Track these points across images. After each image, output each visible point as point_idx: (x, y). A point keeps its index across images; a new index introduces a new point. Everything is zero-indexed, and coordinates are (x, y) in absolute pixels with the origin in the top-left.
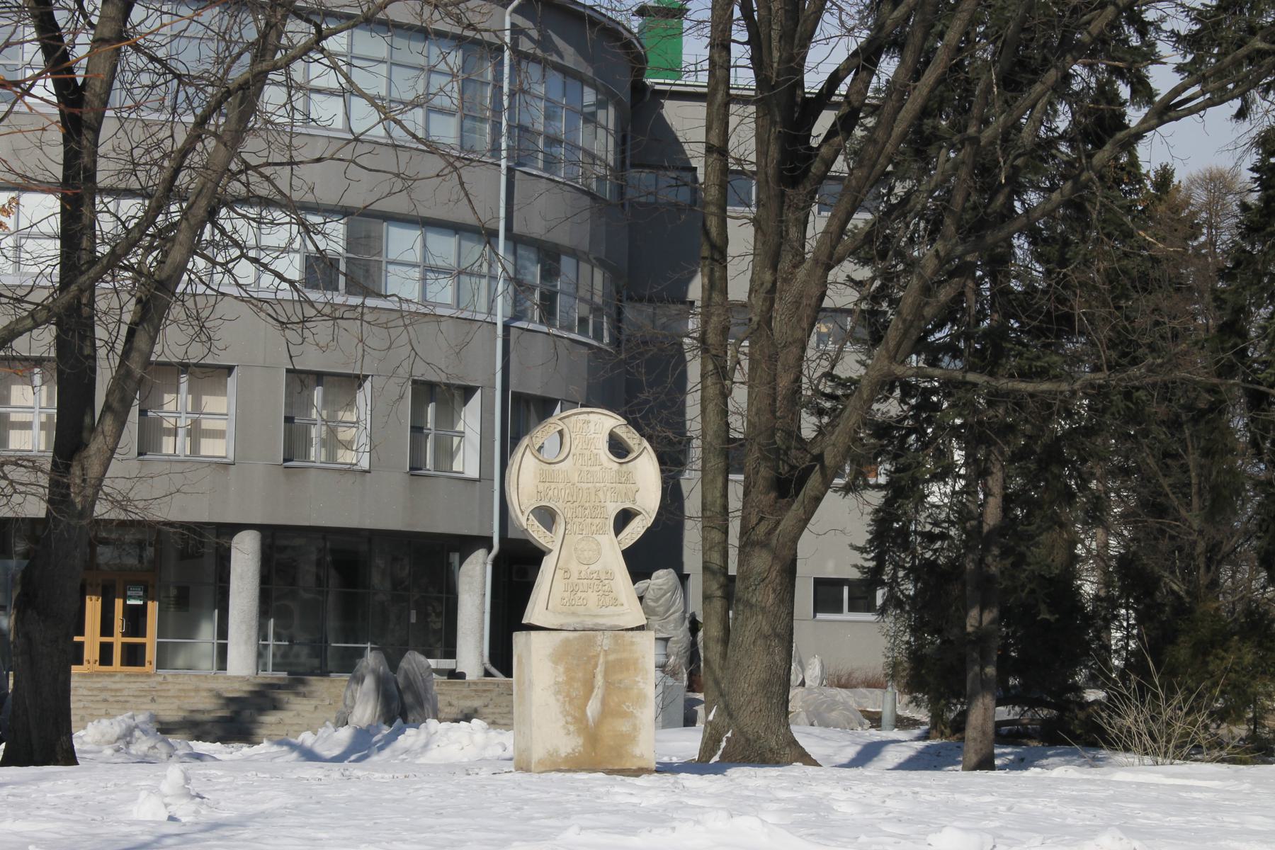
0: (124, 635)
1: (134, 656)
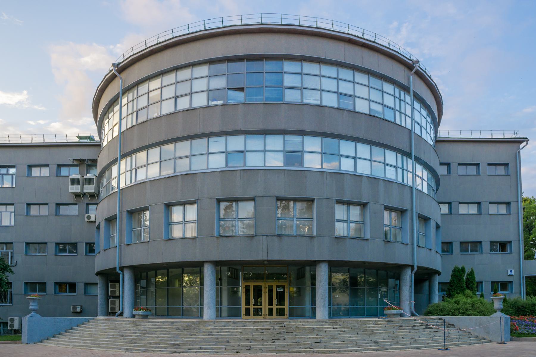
0: (254, 305)
1: (281, 312)
